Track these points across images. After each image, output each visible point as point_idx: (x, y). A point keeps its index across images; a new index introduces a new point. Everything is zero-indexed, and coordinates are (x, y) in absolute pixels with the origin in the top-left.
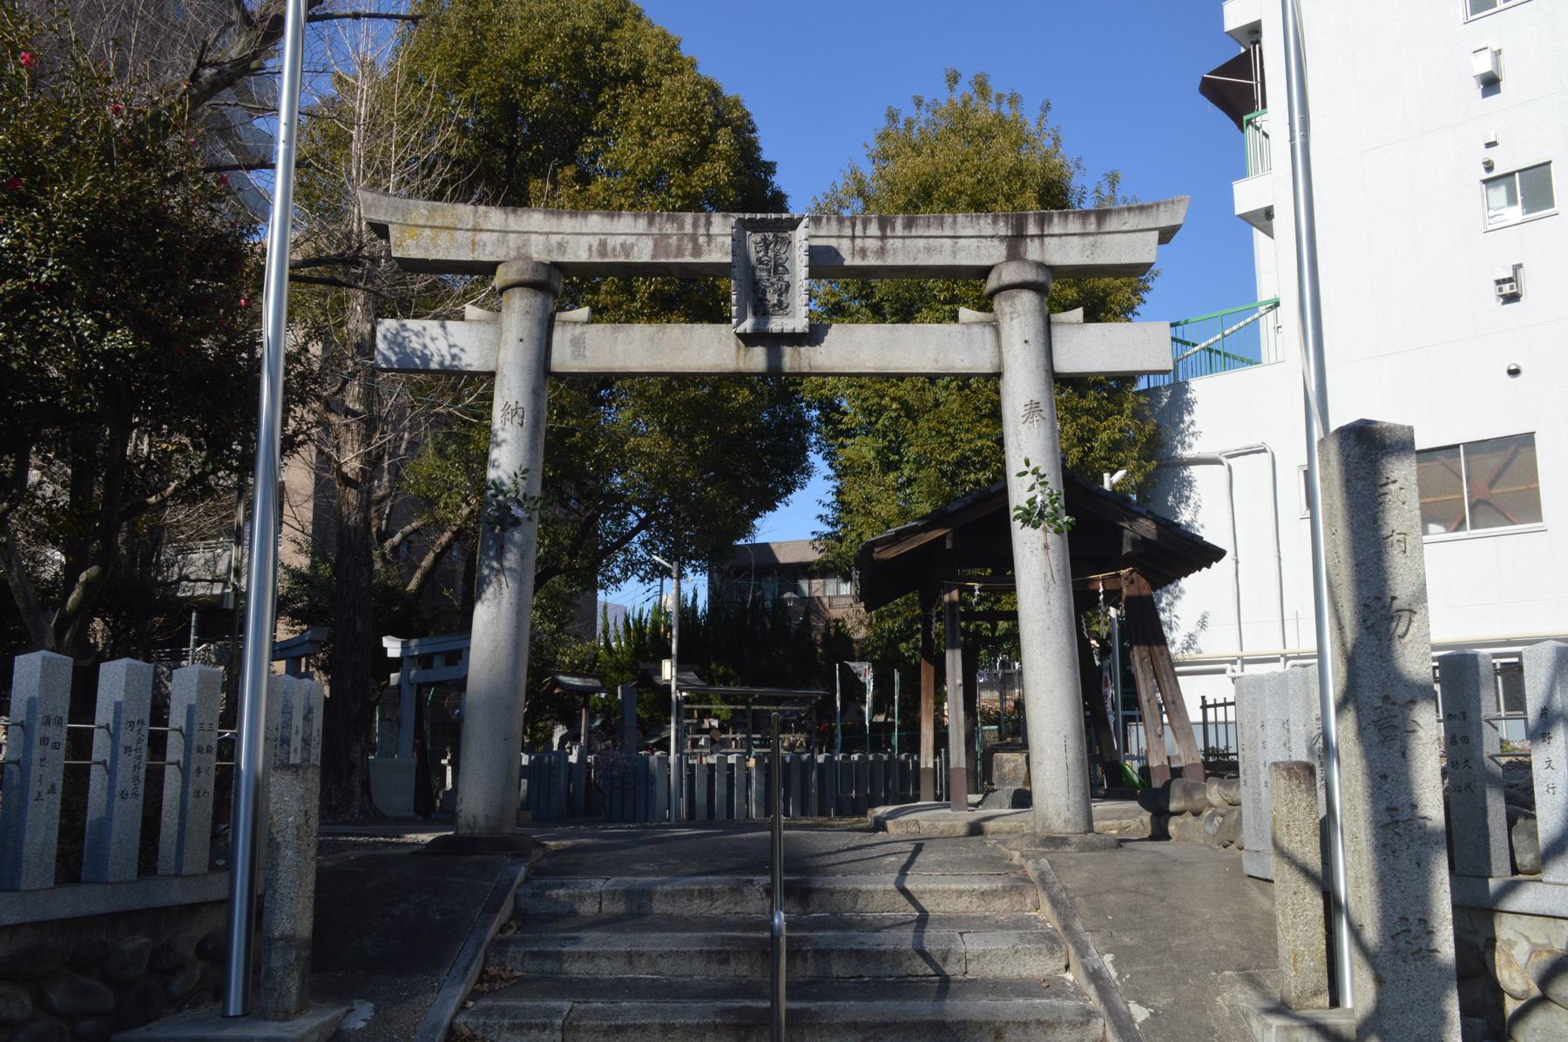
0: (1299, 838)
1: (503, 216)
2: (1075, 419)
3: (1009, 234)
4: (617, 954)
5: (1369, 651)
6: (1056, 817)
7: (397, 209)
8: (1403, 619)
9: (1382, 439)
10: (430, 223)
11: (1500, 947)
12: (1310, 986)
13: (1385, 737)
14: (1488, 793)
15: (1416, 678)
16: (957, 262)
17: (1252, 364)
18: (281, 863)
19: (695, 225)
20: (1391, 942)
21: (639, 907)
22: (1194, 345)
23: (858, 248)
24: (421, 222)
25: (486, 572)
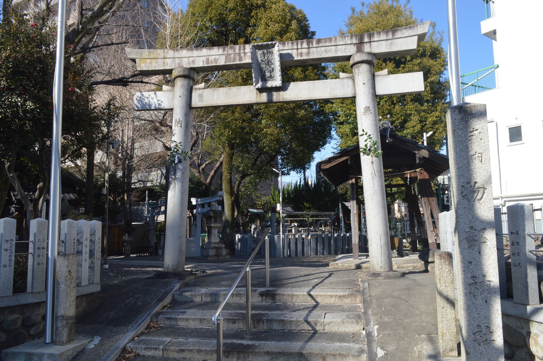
0: (445, 284)
1: (173, 52)
2: (419, 114)
3: (357, 42)
4: (196, 319)
5: (464, 206)
6: (377, 266)
7: (138, 53)
8: (480, 192)
9: (471, 111)
10: (149, 57)
11: (532, 336)
12: (449, 347)
13: (471, 245)
14: (528, 268)
15: (486, 218)
16: (337, 55)
17: (488, 89)
18: (60, 289)
19: (240, 50)
20: (473, 336)
21: (215, 299)
22: (467, 84)
23: (299, 53)
24: (146, 57)
25: (170, 180)
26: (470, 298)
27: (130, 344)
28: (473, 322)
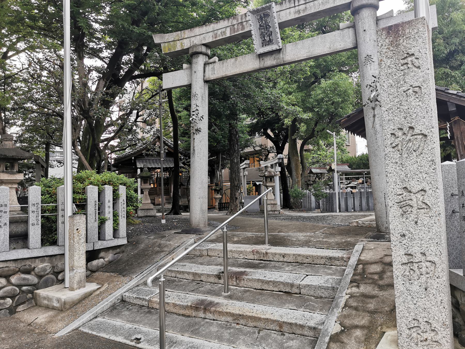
5: (394, 161)
16: (335, 5)
26: (404, 282)
27: (127, 293)
28: (408, 315)
